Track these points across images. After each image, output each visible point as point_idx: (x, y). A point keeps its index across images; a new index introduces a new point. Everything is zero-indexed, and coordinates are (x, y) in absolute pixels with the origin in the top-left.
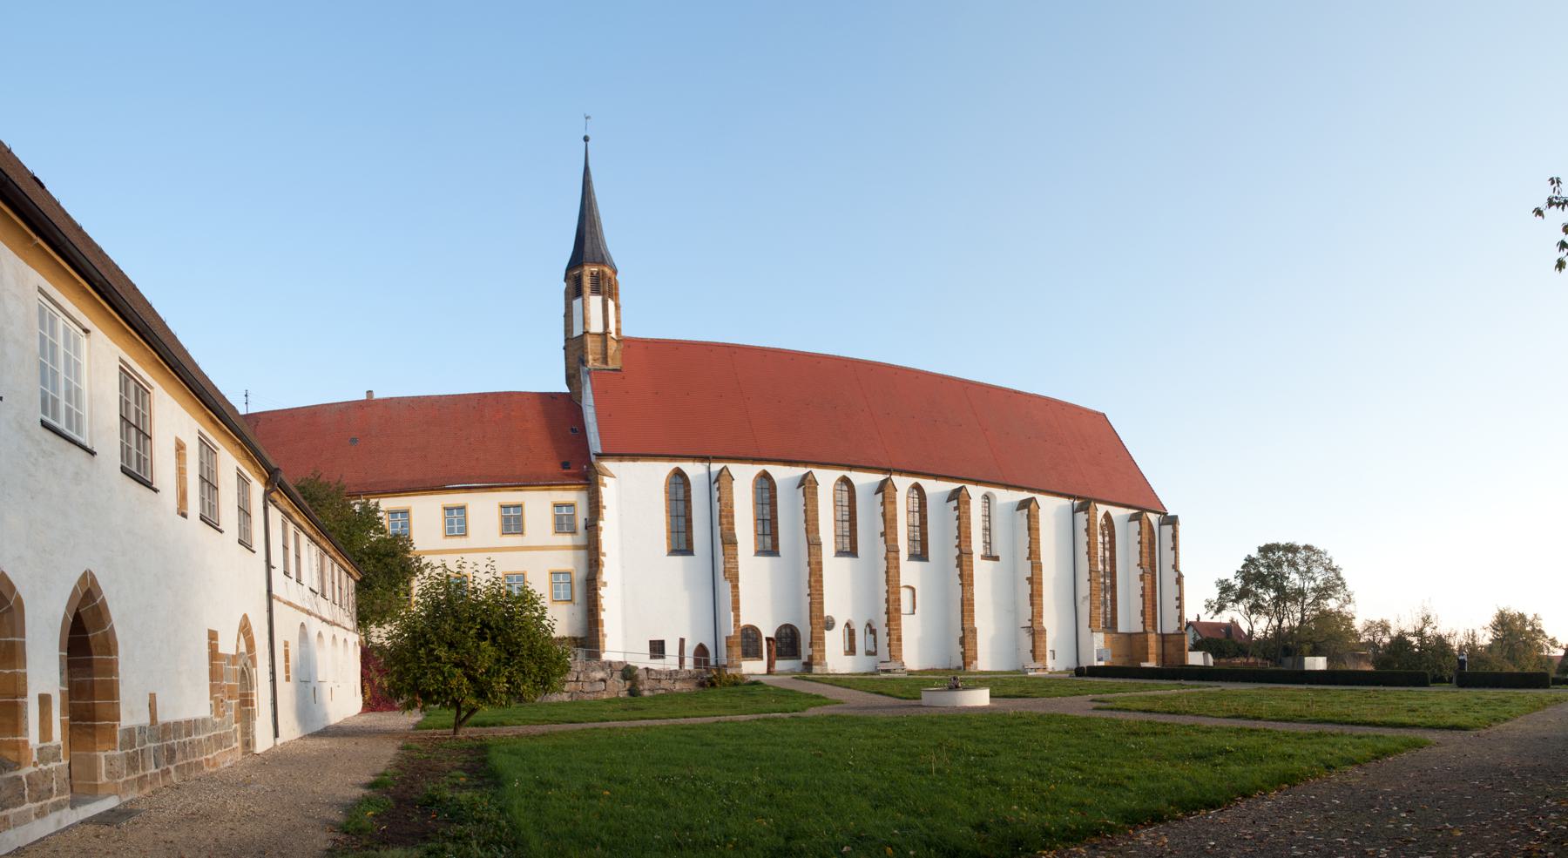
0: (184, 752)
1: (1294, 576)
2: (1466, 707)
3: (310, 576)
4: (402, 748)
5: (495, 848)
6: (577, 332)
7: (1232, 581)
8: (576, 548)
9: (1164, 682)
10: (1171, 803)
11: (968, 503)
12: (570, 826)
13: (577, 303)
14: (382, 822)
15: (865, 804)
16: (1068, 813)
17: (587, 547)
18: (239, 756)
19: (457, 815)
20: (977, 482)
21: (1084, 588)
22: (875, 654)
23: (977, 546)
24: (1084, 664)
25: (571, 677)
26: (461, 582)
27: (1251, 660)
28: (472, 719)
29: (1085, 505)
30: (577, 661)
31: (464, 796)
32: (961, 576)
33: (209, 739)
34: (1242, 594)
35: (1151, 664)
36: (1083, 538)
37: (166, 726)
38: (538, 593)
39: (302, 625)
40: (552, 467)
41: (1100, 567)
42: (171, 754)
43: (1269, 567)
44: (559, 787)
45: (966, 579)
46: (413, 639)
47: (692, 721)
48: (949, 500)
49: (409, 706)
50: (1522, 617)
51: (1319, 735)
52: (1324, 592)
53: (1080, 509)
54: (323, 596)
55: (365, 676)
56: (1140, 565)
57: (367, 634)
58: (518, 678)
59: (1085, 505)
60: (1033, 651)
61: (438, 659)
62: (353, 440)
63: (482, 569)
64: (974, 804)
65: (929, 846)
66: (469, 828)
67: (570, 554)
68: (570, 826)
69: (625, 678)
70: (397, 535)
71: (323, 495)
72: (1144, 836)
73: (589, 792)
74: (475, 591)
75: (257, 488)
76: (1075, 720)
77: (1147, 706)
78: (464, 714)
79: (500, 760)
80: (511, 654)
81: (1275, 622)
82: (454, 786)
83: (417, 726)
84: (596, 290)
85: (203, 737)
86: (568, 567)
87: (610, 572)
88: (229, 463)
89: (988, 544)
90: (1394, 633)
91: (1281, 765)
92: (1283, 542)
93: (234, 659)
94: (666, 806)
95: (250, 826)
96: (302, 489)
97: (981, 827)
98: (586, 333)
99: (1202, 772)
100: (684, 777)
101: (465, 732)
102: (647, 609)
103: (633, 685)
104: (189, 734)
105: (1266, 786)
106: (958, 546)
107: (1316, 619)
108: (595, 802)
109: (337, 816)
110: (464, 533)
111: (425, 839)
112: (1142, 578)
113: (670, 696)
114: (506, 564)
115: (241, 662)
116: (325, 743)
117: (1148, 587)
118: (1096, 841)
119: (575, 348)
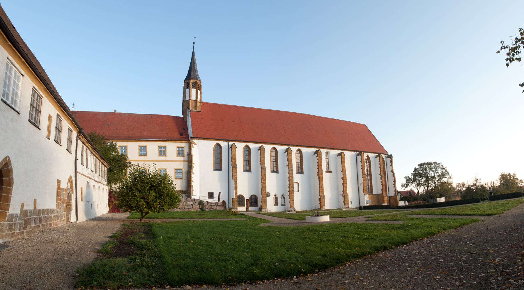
0: (45, 220)
1: (431, 172)
2: (494, 207)
3: (91, 166)
4: (122, 225)
5: (153, 258)
6: (187, 99)
7: (410, 177)
8: (184, 161)
9: (391, 210)
10: (390, 243)
12: (179, 252)
13: (188, 90)
14: (115, 249)
15: (284, 250)
16: (355, 249)
17: (188, 161)
18: (65, 223)
19: (141, 247)
20: (324, 148)
21: (361, 180)
22: (285, 205)
23: (324, 168)
24: (362, 205)
25: (181, 203)
26: (144, 171)
27: (419, 202)
28: (147, 216)
29: (360, 153)
30: (183, 198)
31: (143, 241)
32: (319, 178)
33: (55, 216)
34: (414, 181)
35: (386, 204)
36: (360, 164)
37: (39, 210)
38: (170, 176)
39: (88, 182)
40: (177, 135)
41: (366, 173)
42: (41, 220)
43: (422, 170)
44: (176, 239)
45: (321, 179)
46: (127, 189)
47: (222, 219)
48: (314, 154)
49: (125, 211)
50: (509, 175)
51: (440, 219)
52: (442, 176)
53: (359, 155)
54: (96, 173)
55: (110, 201)
56: (380, 174)
57: (111, 187)
58: (163, 203)
59: (360, 153)
60: (344, 202)
61: (135, 196)
62: (108, 124)
63: (152, 167)
64: (322, 248)
65: (306, 264)
66: (145, 252)
67: (182, 163)
68: (179, 252)
69: (199, 204)
70: (122, 154)
71: (97, 139)
72: (381, 255)
73: (186, 241)
74: (149, 174)
75: (75, 134)
76: (360, 224)
77: (385, 218)
78: (144, 214)
79: (156, 230)
80: (161, 195)
81: (426, 188)
82: (140, 238)
83: (128, 218)
84: (194, 87)
85: (53, 215)
86: (181, 167)
87: (196, 170)
88: (66, 125)
89: (328, 167)
90: (467, 186)
91: (428, 229)
92: (426, 162)
93: (65, 190)
94: (212, 247)
95: (67, 246)
96: (90, 136)
97: (325, 256)
98: (190, 99)
99: (401, 233)
100: (219, 238)
101: (144, 220)
102: (207, 184)
103: (202, 207)
104: (48, 214)
105: (423, 237)
106: (318, 169)
107: (440, 185)
108: (188, 244)
109: (99, 247)
110: (146, 155)
111: (130, 255)
112: (381, 179)
113: (215, 211)
114: (160, 166)
115: (68, 191)
116: (95, 223)
117: (384, 181)
118: (365, 257)
119: (186, 104)
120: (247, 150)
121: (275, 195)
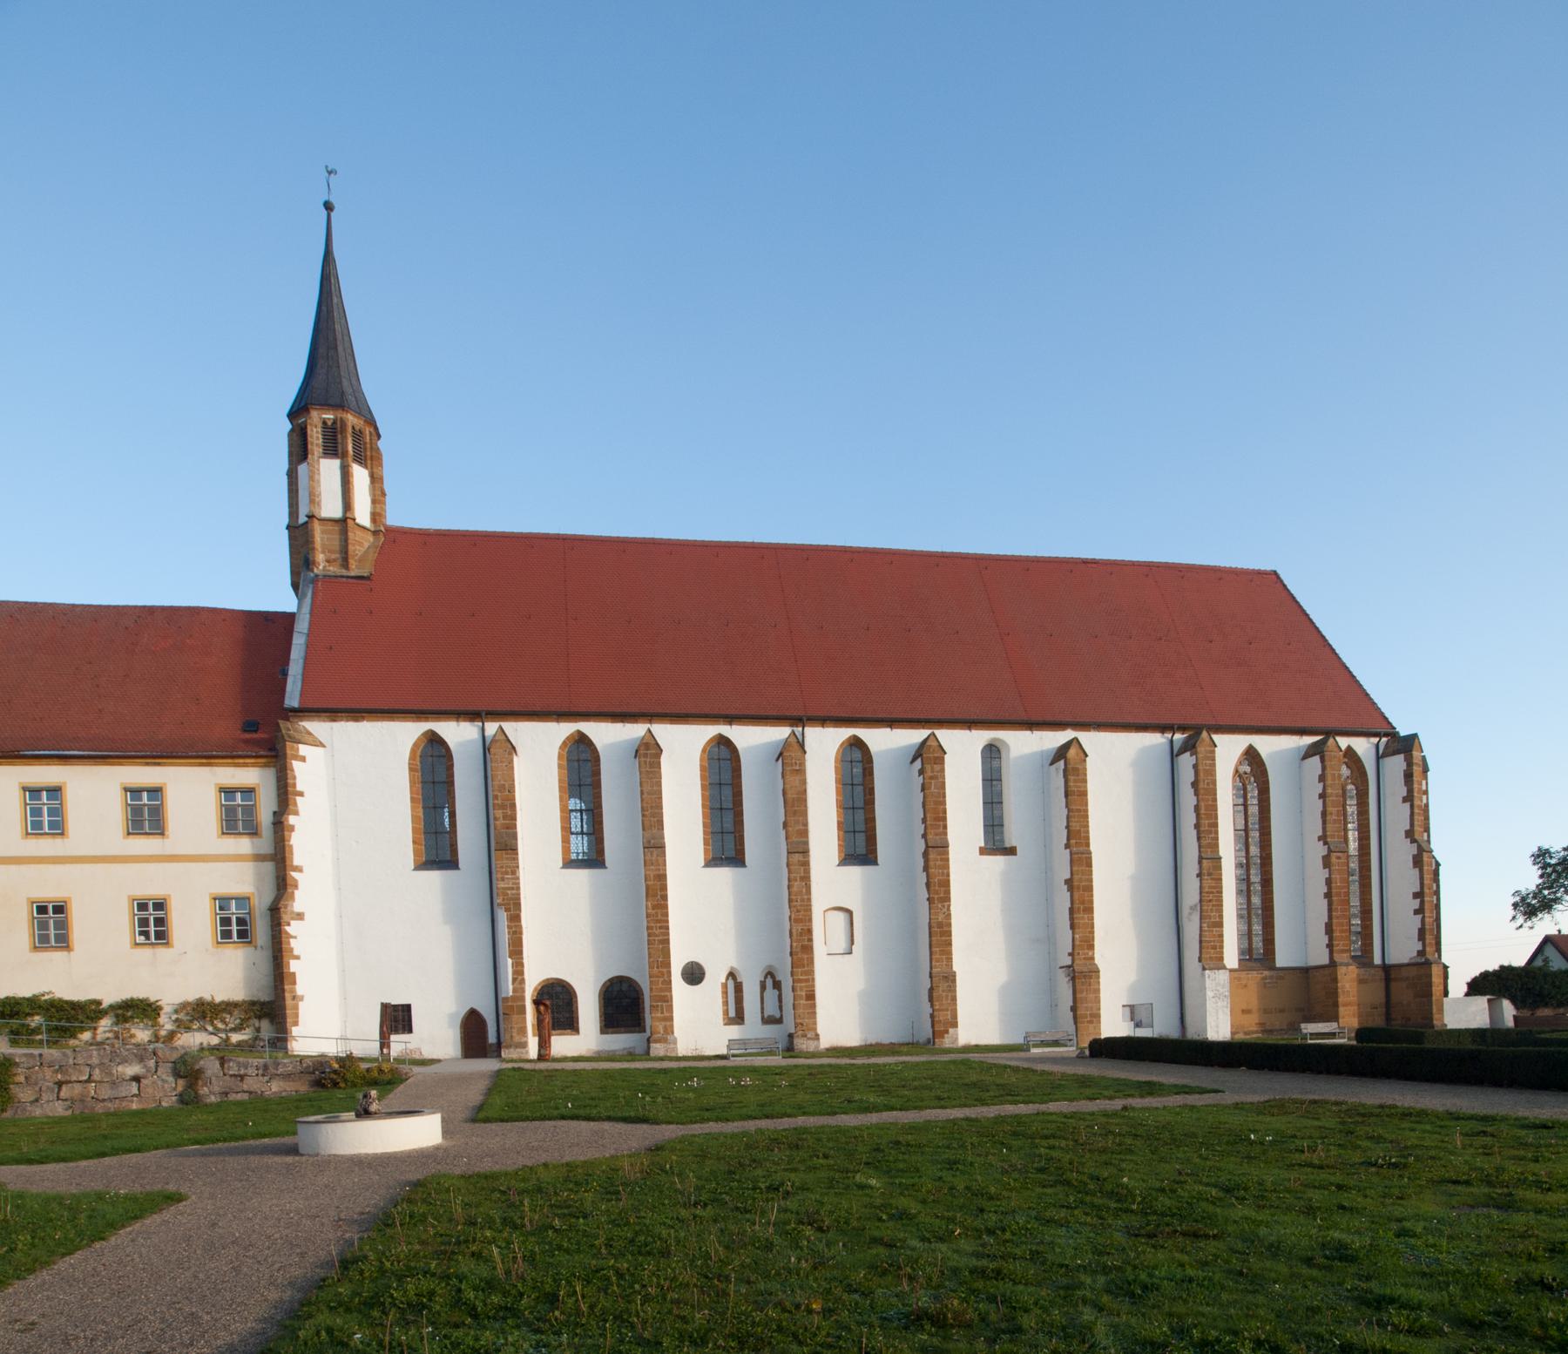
8: (259, 858)
11: (941, 761)
22: (779, 1021)
36: (1188, 799)
40: (227, 728)
45: (938, 890)
53: (1190, 746)
69: (177, 1074)
120: (857, 760)
121: (732, 975)
